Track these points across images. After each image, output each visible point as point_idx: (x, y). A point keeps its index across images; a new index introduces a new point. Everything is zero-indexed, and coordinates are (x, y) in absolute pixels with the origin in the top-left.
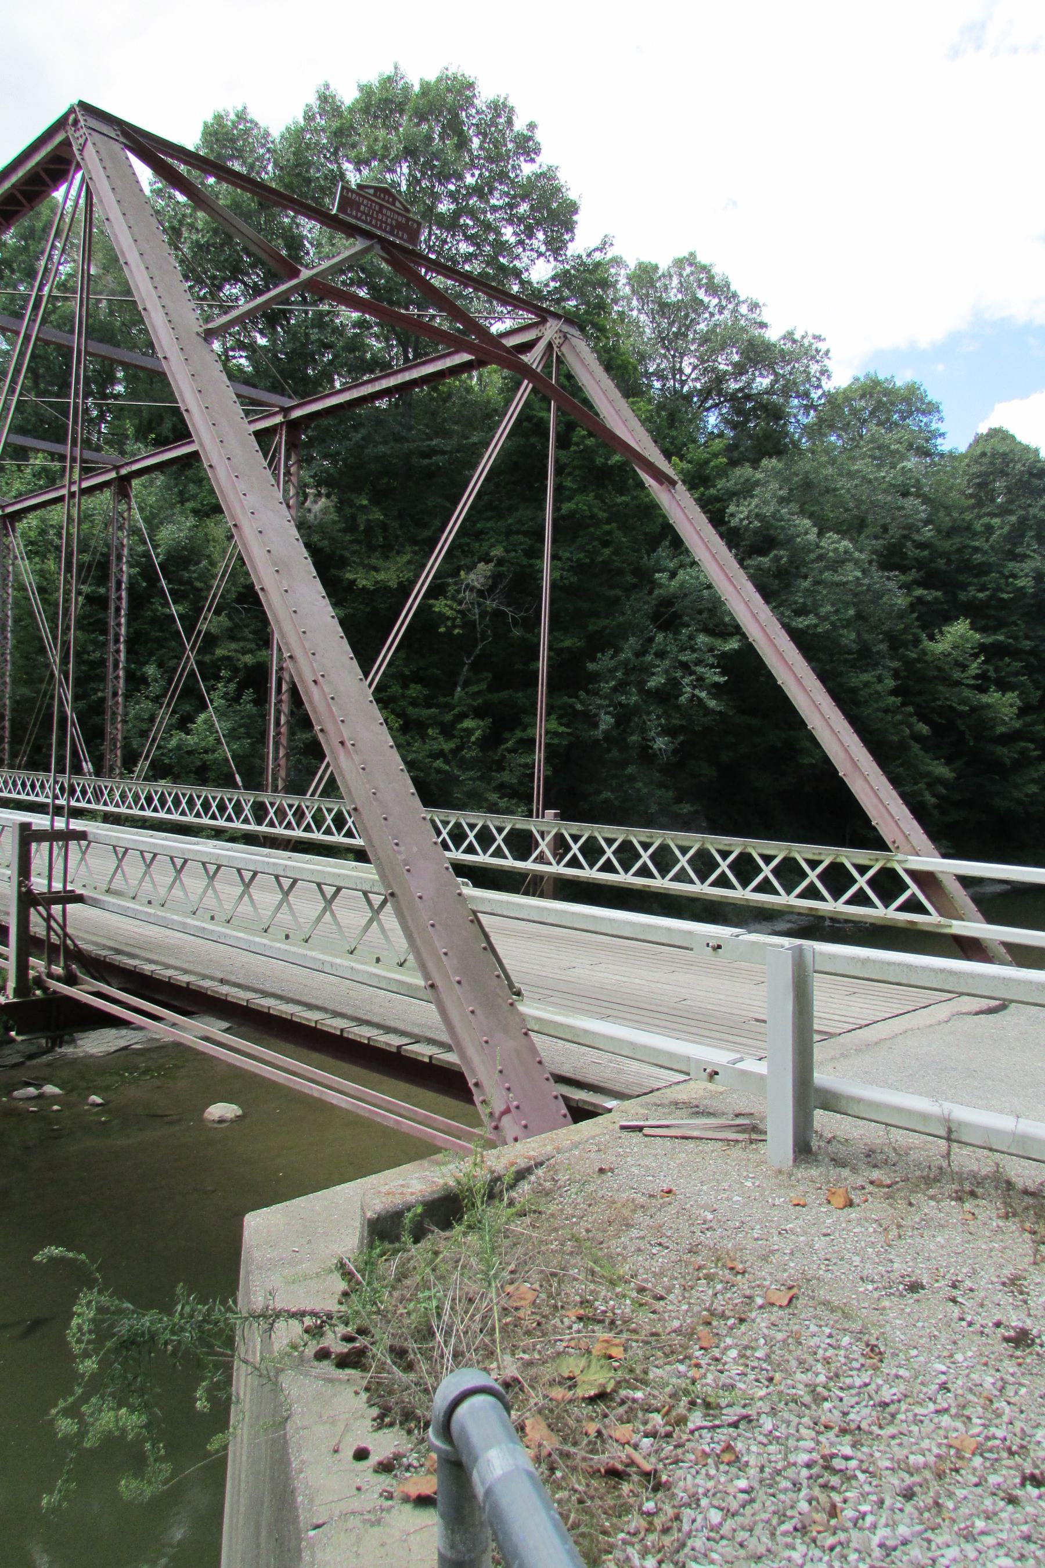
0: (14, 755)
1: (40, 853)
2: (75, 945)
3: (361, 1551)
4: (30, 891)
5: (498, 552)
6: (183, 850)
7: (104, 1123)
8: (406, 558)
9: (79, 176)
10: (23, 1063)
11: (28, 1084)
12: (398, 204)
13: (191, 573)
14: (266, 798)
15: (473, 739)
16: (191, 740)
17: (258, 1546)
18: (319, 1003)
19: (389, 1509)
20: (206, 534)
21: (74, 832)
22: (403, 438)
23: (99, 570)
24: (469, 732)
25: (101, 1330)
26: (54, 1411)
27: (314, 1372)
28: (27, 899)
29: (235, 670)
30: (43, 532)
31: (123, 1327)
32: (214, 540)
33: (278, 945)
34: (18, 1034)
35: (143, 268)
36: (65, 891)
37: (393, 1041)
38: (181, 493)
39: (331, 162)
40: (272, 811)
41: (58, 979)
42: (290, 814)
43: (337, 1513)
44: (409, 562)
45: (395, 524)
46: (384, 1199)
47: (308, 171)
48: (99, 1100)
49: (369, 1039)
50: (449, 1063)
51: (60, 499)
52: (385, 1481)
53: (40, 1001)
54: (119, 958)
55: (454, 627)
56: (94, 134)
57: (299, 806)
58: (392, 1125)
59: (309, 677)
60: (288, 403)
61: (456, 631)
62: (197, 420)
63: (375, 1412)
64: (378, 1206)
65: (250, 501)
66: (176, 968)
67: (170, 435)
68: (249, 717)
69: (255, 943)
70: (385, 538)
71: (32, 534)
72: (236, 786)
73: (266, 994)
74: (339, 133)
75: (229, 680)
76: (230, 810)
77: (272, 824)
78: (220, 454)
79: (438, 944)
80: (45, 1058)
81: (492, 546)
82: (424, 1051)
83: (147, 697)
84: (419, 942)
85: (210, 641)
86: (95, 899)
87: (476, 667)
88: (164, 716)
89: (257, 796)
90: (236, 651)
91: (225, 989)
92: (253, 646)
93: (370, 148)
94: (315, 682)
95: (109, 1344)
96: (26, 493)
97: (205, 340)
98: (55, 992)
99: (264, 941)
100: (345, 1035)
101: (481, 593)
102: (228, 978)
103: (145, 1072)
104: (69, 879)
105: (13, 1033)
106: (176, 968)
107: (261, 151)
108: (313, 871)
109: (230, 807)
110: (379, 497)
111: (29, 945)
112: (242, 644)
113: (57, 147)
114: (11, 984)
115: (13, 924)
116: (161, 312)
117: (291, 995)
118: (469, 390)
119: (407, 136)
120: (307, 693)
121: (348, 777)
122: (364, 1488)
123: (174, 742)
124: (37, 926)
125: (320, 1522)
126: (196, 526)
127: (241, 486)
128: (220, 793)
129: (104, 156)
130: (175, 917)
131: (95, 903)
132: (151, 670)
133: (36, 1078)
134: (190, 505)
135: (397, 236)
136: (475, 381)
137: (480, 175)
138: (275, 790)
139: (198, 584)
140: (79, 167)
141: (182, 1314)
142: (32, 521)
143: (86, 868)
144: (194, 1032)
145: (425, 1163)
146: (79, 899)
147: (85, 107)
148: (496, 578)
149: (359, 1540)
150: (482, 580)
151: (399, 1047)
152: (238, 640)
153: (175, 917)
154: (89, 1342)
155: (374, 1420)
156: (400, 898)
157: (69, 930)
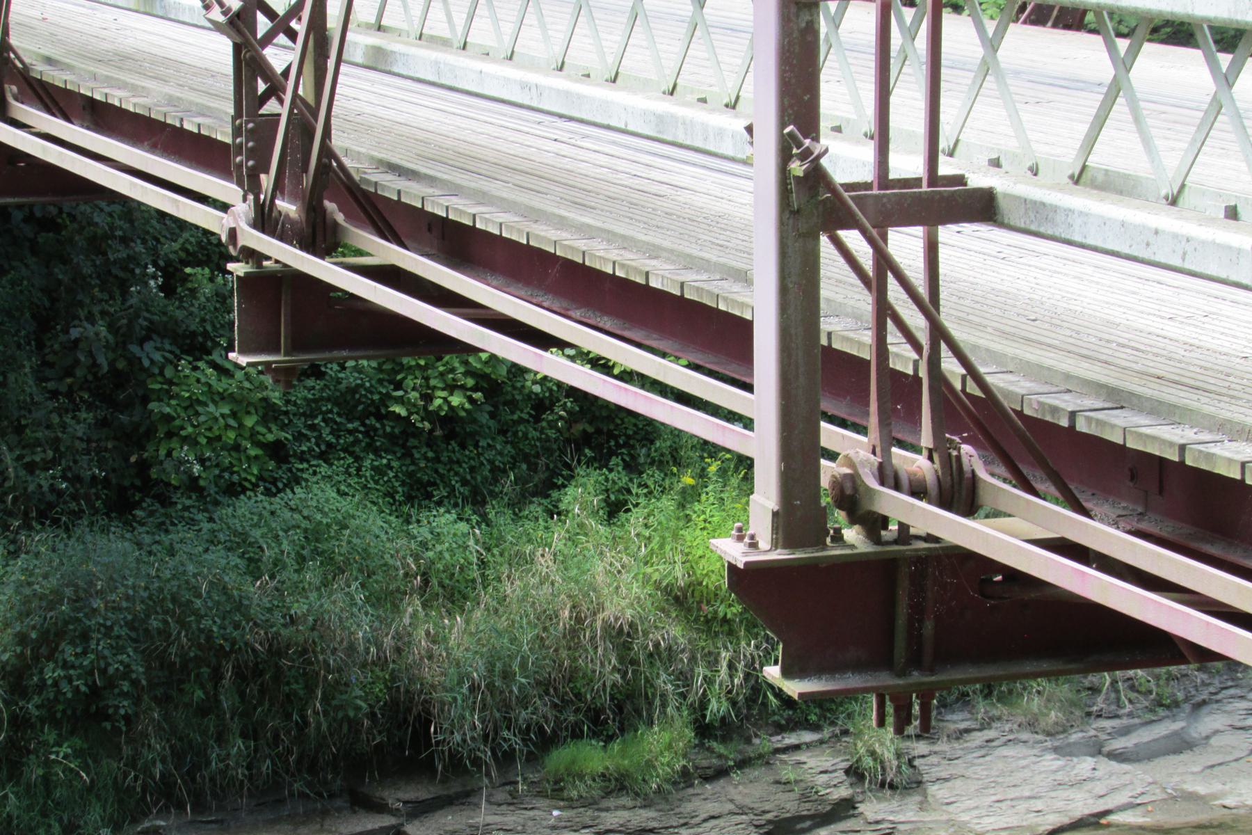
4: (817, 177)
23: (926, 727)
28: (811, 205)
34: (787, 673)
36: (933, 178)
41: (918, 491)
53: (856, 564)
54: (1121, 419)
86: (1038, 207)
98: (904, 533)
104: (943, 144)
111: (824, 380)
114: (766, 497)
115: (761, 307)
124: (845, 317)
146: (982, 207)
157: (947, 318)
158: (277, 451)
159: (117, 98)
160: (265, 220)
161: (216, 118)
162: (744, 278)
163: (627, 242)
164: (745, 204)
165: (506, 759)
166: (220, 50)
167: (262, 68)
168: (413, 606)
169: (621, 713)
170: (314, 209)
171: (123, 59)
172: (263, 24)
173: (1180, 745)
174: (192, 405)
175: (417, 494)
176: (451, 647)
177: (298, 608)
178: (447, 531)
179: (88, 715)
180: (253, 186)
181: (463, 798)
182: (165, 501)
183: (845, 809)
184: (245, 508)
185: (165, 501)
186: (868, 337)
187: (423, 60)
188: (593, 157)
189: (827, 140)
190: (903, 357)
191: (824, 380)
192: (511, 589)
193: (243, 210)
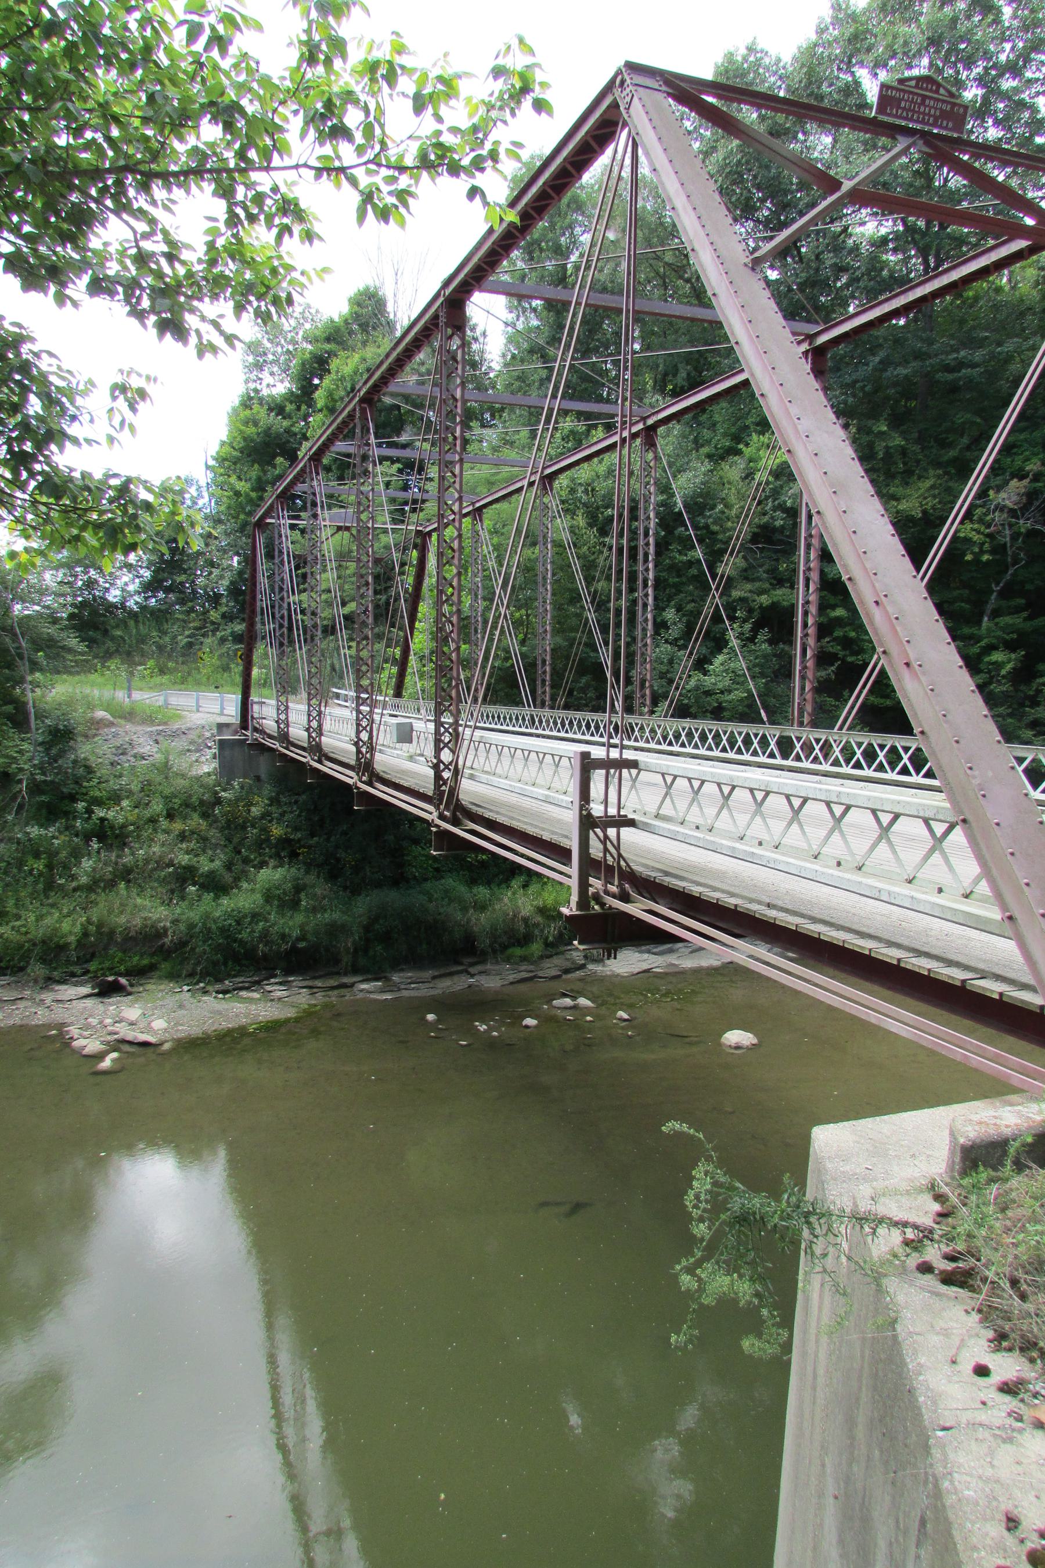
0: (553, 699)
1: (598, 777)
2: (628, 865)
3: (995, 1462)
4: (589, 815)
5: (1033, 466)
6: (731, 778)
7: (630, 1037)
8: (928, 483)
9: (624, 135)
10: (559, 976)
11: (565, 995)
12: (942, 91)
13: (708, 518)
14: (792, 732)
15: (1003, 672)
16: (709, 681)
17: (852, 1438)
18: (871, 931)
19: (1021, 1431)
20: (721, 478)
21: (627, 760)
22: (925, 353)
24: (998, 665)
25: (717, 1205)
26: (678, 1267)
27: (918, 1283)
28: (587, 822)
29: (750, 611)
30: (573, 491)
31: (736, 1204)
32: (729, 483)
33: (831, 871)
35: (690, 209)
37: (957, 975)
38: (696, 441)
39: (845, 73)
40: (798, 746)
41: (614, 896)
42: (817, 748)
43: (964, 1421)
44: (932, 487)
45: (917, 448)
46: (977, 1128)
47: (819, 88)
48: (625, 1016)
49: (929, 970)
50: (1022, 1001)
51: (613, 446)
52: (1008, 1402)
53: (597, 915)
54: (667, 879)
55: (982, 552)
56: (639, 89)
57: (826, 741)
58: (958, 1058)
59: (870, 599)
60: (813, 329)
61: (985, 557)
62: (747, 350)
63: (991, 1334)
64: (970, 1133)
65: (804, 425)
66: (723, 891)
67: (685, 384)
68: (765, 656)
69: (805, 869)
70: (905, 464)
71: (563, 493)
72: (763, 723)
73: (815, 920)
74: (855, 38)
75: (745, 621)
76: (755, 744)
77: (798, 758)
78: (772, 381)
79: (1019, 874)
80: (579, 974)
81: (1027, 459)
82: (993, 988)
83: (667, 641)
84: (994, 872)
85: (730, 583)
86: (646, 824)
87: (1003, 595)
88: (685, 660)
89: (783, 730)
90: (750, 591)
91: (772, 913)
92: (767, 586)
93: (889, 47)
94: (877, 603)
95: (723, 1217)
96: (557, 457)
97: (753, 269)
98: (610, 907)
99: (817, 867)
100: (902, 965)
101: (1012, 513)
102: (774, 902)
103: (666, 995)
105: (575, 943)
106: (723, 891)
107: (773, 79)
108: (869, 799)
109: (755, 742)
110: (897, 421)
111: (590, 866)
112: (757, 584)
113: (605, 112)
114: (574, 898)
116: (709, 249)
117: (841, 923)
118: (999, 290)
119: (929, 24)
120: (867, 614)
121: (914, 700)
122: (990, 1403)
123: (693, 683)
124: (596, 850)
125: (948, 1425)
126: (711, 471)
127: (794, 410)
128: (745, 728)
129: (648, 108)
130: (724, 842)
131: (646, 828)
132: (670, 614)
133: (572, 991)
134: (705, 450)
135: (941, 127)
136: (1005, 280)
137: (1012, 49)
138: (801, 724)
139: (715, 528)
140: (625, 124)
141: (788, 1202)
142: (563, 481)
143: (638, 797)
144: (745, 952)
145: (997, 1102)
146: (632, 823)
147: (632, 67)
148: (1031, 496)
149: (991, 1453)
150: (1015, 498)
151: (964, 981)
152: (753, 580)
153: (724, 842)
154: (705, 1210)
155: (990, 1341)
156: (974, 825)
158: (437, 870)
159: (402, 782)
160: (441, 817)
161: (429, 789)
162: (570, 839)
163: (536, 827)
164: (571, 817)
165: (494, 951)
166: (431, 773)
167: (442, 778)
168: (471, 911)
169: (526, 939)
170: (454, 814)
171: (404, 772)
172: (442, 767)
173: (671, 951)
174: (415, 857)
175: (473, 882)
176: (480, 921)
177: (442, 910)
178: (482, 892)
179: (386, 938)
180: (437, 808)
181: (483, 962)
182: (408, 882)
183: (583, 967)
184: (428, 885)
185: (408, 882)
186: (601, 855)
187: (484, 777)
188: (526, 803)
189: (592, 805)
190: (610, 860)
191: (590, 866)
192: (497, 907)
193: (436, 814)
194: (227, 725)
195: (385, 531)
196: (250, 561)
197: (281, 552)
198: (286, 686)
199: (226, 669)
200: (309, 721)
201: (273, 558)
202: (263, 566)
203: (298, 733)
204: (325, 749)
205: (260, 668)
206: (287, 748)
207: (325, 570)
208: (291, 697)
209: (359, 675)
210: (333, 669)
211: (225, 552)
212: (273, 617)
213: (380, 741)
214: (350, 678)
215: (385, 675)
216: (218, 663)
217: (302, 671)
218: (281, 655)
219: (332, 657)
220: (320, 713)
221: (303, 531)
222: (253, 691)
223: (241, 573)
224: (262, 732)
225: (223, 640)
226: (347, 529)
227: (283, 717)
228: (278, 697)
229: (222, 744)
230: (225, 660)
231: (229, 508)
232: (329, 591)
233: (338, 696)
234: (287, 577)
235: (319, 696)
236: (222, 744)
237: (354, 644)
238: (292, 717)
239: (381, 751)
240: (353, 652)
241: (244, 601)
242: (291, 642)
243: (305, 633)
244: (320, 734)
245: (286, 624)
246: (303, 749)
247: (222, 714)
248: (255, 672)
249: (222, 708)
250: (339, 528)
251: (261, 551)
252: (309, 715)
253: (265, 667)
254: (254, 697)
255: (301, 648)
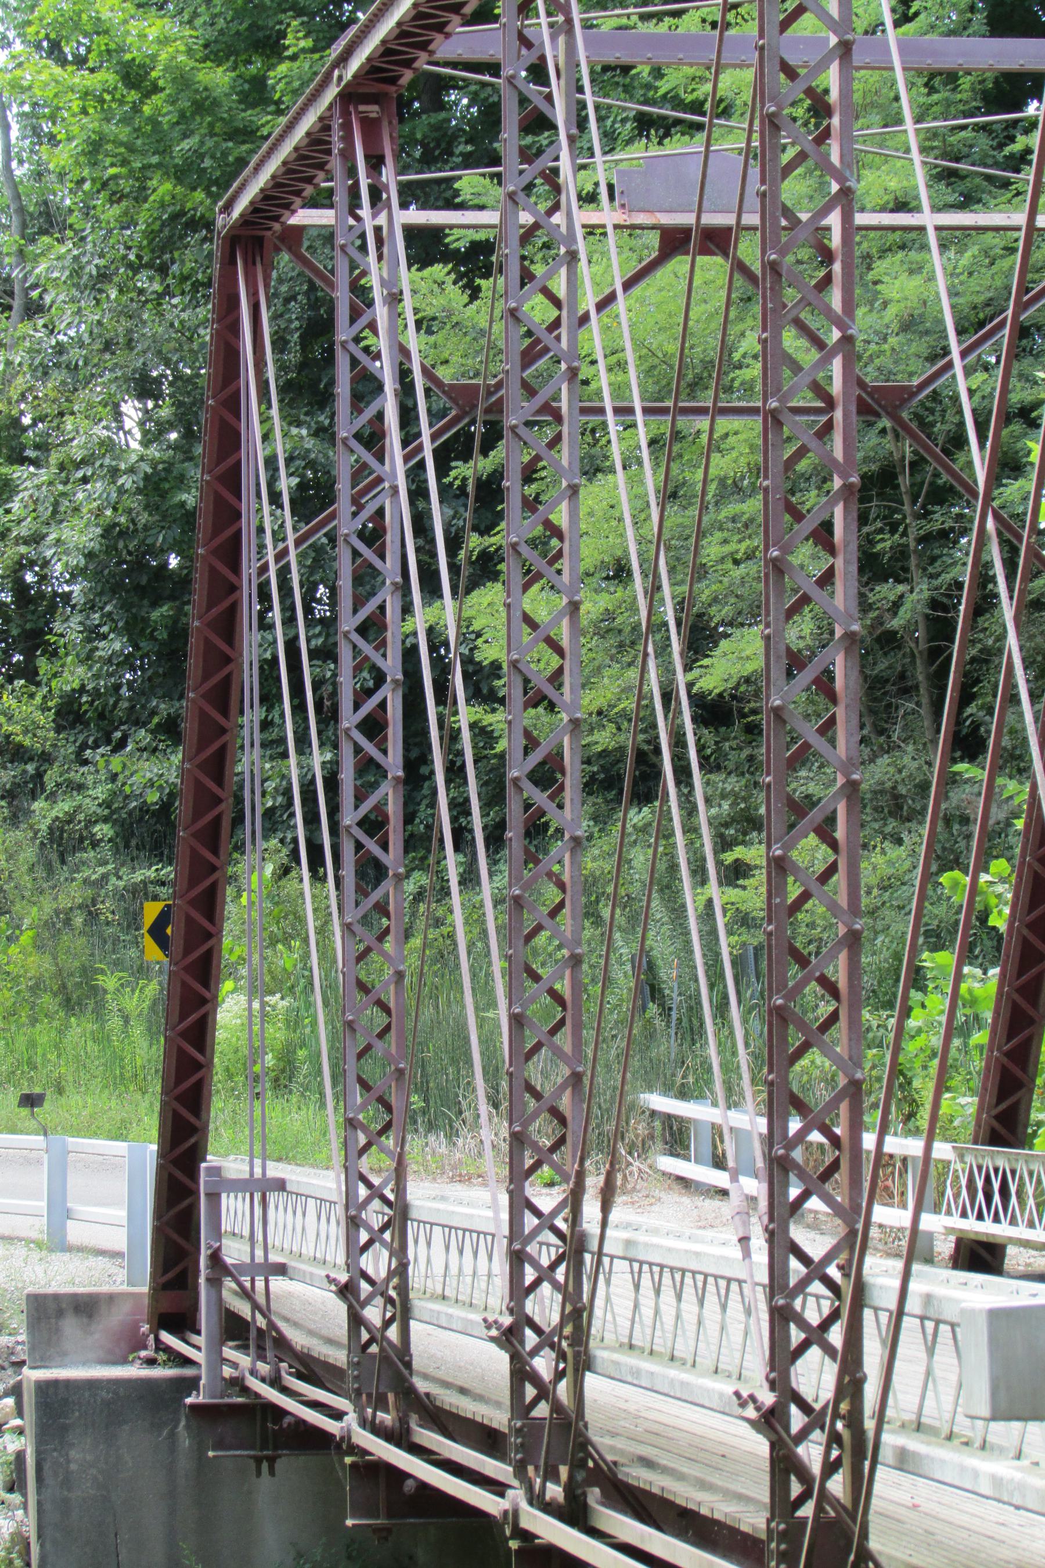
146: (281, 1270)
172: (797, 1419)
194: (86, 1306)
195: (910, 239)
196: (212, 425)
197: (367, 387)
198: (394, 1091)
199: (78, 996)
200: (519, 1291)
201: (324, 399)
202: (268, 435)
203: (457, 1350)
204: (607, 1444)
205: (256, 989)
206: (400, 1437)
207: (594, 468)
208: (422, 1147)
209: (783, 1040)
210: (650, 988)
211: (78, 377)
212: (329, 715)
213: (904, 1399)
214: (734, 1039)
215: (930, 1011)
216: (38, 964)
217: (483, 1014)
218: (373, 925)
219: (639, 920)
220: (575, 1247)
221: (475, 262)
222: (223, 1112)
223: (157, 485)
224: (269, 1342)
225: (64, 843)
226: (717, 240)
227: (377, 1263)
228: (354, 1153)
229: (56, 1407)
230: (75, 945)
231: (94, 148)
232: (620, 573)
233: (676, 1136)
234: (399, 511)
235: (570, 1137)
236: (56, 1407)
237: (754, 853)
238: (429, 1262)
239: (904, 1461)
240: (752, 895)
241: (178, 633)
242: (420, 844)
243: (495, 794)
244: (579, 1362)
245: (394, 760)
246: (489, 1440)
247: (56, 1242)
248: (231, 1010)
249: (60, 1212)
250: (674, 242)
251: (260, 368)
252: (517, 1259)
253: (279, 983)
254: (226, 1157)
255: (469, 879)
